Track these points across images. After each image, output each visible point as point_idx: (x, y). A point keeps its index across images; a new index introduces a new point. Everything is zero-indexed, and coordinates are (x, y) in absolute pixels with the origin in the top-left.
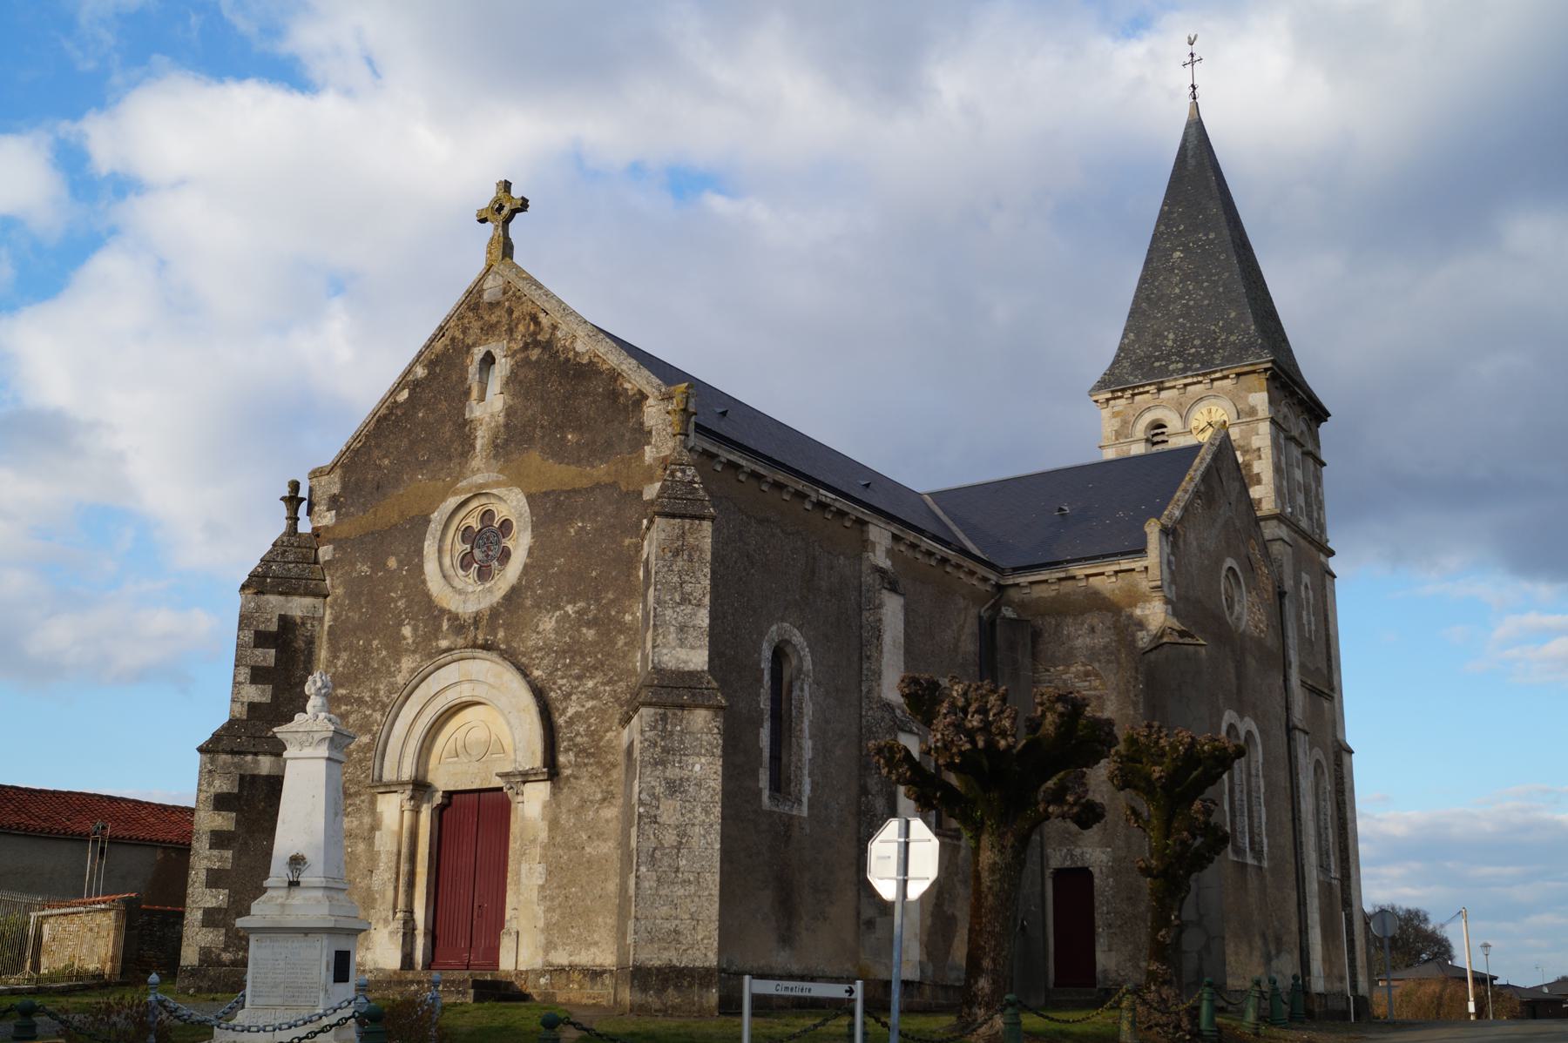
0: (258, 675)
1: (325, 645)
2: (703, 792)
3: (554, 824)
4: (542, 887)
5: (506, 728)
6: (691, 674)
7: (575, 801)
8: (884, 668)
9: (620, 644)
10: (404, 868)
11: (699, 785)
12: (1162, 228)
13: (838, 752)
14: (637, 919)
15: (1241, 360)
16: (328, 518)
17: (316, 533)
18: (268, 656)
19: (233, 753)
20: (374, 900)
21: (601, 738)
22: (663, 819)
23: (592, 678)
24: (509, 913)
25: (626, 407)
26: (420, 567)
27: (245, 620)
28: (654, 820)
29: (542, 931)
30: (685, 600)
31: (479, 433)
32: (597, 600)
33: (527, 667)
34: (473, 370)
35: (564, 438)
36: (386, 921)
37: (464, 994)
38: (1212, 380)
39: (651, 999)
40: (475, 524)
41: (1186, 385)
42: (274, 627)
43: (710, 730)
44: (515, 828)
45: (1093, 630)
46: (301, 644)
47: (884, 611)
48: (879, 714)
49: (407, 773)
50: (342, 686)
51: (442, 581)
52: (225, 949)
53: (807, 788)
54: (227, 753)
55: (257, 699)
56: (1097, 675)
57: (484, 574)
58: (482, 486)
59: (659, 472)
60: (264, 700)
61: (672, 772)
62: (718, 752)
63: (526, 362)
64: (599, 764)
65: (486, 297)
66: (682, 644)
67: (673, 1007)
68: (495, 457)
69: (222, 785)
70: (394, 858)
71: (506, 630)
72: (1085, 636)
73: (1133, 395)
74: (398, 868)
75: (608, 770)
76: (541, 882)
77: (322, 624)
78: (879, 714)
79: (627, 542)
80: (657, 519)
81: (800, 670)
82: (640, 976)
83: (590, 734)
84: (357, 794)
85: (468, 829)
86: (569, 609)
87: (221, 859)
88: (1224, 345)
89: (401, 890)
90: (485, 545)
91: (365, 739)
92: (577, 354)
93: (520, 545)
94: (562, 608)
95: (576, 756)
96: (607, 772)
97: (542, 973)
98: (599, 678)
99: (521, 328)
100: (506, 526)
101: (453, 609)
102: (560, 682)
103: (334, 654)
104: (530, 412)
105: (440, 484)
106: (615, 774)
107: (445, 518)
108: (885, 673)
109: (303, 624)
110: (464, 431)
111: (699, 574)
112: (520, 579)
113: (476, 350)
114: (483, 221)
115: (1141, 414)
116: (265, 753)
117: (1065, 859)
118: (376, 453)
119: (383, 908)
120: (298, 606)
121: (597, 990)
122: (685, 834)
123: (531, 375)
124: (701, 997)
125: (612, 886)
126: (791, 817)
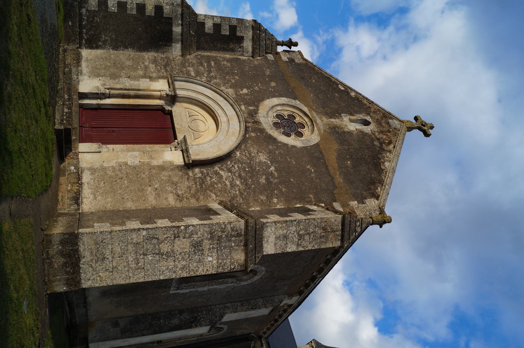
0: (217, 27)
1: (232, 57)
2: (195, 264)
3: (162, 168)
4: (126, 164)
5: (207, 140)
7: (175, 179)
10: (132, 93)
11: (200, 261)
13: (200, 300)
14: (111, 232)
16: (285, 58)
17: (277, 53)
18: (225, 31)
19: (182, 14)
20: (115, 79)
21: (211, 191)
23: (241, 183)
24: (111, 147)
25: (370, 189)
29: (102, 166)
30: (301, 237)
31: (337, 120)
32: (280, 183)
33: (240, 148)
35: (348, 159)
36: (104, 85)
37: (61, 123)
39: (56, 248)
40: (298, 120)
42: (238, 34)
44: (157, 147)
46: (232, 46)
47: (264, 309)
49: (180, 93)
50: (215, 64)
51: (271, 106)
52: (87, 10)
53: (184, 291)
54: (182, 12)
55: (206, 26)
57: (276, 125)
58: (317, 124)
59: (348, 210)
60: (206, 29)
61: (206, 244)
62: (220, 270)
63: (372, 140)
64: (197, 191)
65: (390, 121)
66: (277, 238)
67: (51, 263)
68: (330, 128)
69: (167, 9)
70: (136, 88)
74: (132, 90)
75: (195, 196)
76: (129, 163)
77: (240, 56)
79: (311, 196)
80: (340, 216)
81: (241, 280)
82: (71, 240)
83: (212, 184)
84: (166, 71)
85: (154, 124)
86: (272, 168)
87: (132, 9)
90: (287, 124)
91: (193, 74)
92: (383, 163)
93: (292, 141)
94: (272, 165)
95: (200, 178)
97: (77, 167)
99: (385, 137)
100: (300, 135)
101: (259, 111)
102: (236, 166)
103: (228, 60)
104: (353, 143)
105: (312, 104)
107: (298, 106)
108: (237, 314)
109: (240, 47)
110: (336, 114)
111: (314, 242)
112: (280, 142)
113: (369, 117)
114: (416, 118)
116: (182, 29)
119: (111, 83)
120: (248, 44)
121: (67, 201)
122: (168, 257)
123: (368, 142)
124: (59, 280)
125: (130, 205)
126: (170, 288)
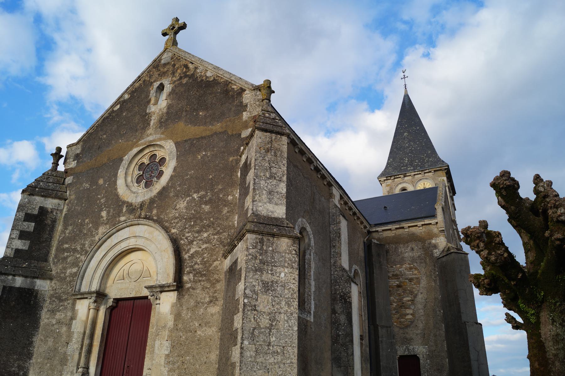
1: (61, 223)
2: (286, 291)
3: (178, 317)
4: (167, 356)
6: (276, 219)
7: (192, 303)
8: (342, 251)
9: (225, 212)
10: (86, 342)
11: (284, 286)
12: (399, 126)
13: (324, 290)
15: (436, 165)
17: (66, 171)
18: (30, 226)
20: (67, 360)
21: (211, 265)
22: (260, 308)
23: (206, 231)
25: (233, 96)
26: (115, 183)
27: (21, 207)
28: (254, 308)
30: (272, 177)
31: (153, 118)
32: (212, 190)
34: (153, 92)
35: (197, 114)
38: (425, 173)
40: (146, 161)
41: (415, 175)
42: (36, 212)
43: (291, 252)
45: (412, 249)
47: (341, 225)
48: (341, 273)
53: (313, 306)
55: (20, 247)
56: (416, 269)
57: (148, 185)
58: (151, 141)
59: (252, 123)
60: (24, 248)
61: (266, 277)
62: (296, 265)
63: (181, 84)
64: (208, 280)
65: (163, 62)
66: (270, 201)
68: (160, 127)
71: (157, 209)
72: (409, 252)
73: (394, 178)
74: (83, 342)
76: (167, 353)
77: (62, 214)
78: (341, 273)
79: (231, 159)
81: (309, 245)
83: (204, 263)
84: (66, 299)
88: (428, 161)
89: (83, 355)
91: (75, 270)
92: (207, 77)
93: (168, 171)
94: (191, 196)
95: (194, 276)
96: (213, 285)
98: (211, 231)
99: (179, 71)
100: (163, 160)
101: (130, 201)
102: (187, 235)
104: (180, 105)
105: (130, 143)
106: (218, 286)
107: (131, 158)
109: (52, 212)
110: (145, 119)
111: (280, 163)
112: (168, 183)
113: (155, 84)
114: (164, 34)
115: (397, 185)
116: (19, 275)
117: (405, 351)
118: (101, 133)
120: (50, 203)
123: (182, 90)
125: (214, 356)
126: (307, 321)
